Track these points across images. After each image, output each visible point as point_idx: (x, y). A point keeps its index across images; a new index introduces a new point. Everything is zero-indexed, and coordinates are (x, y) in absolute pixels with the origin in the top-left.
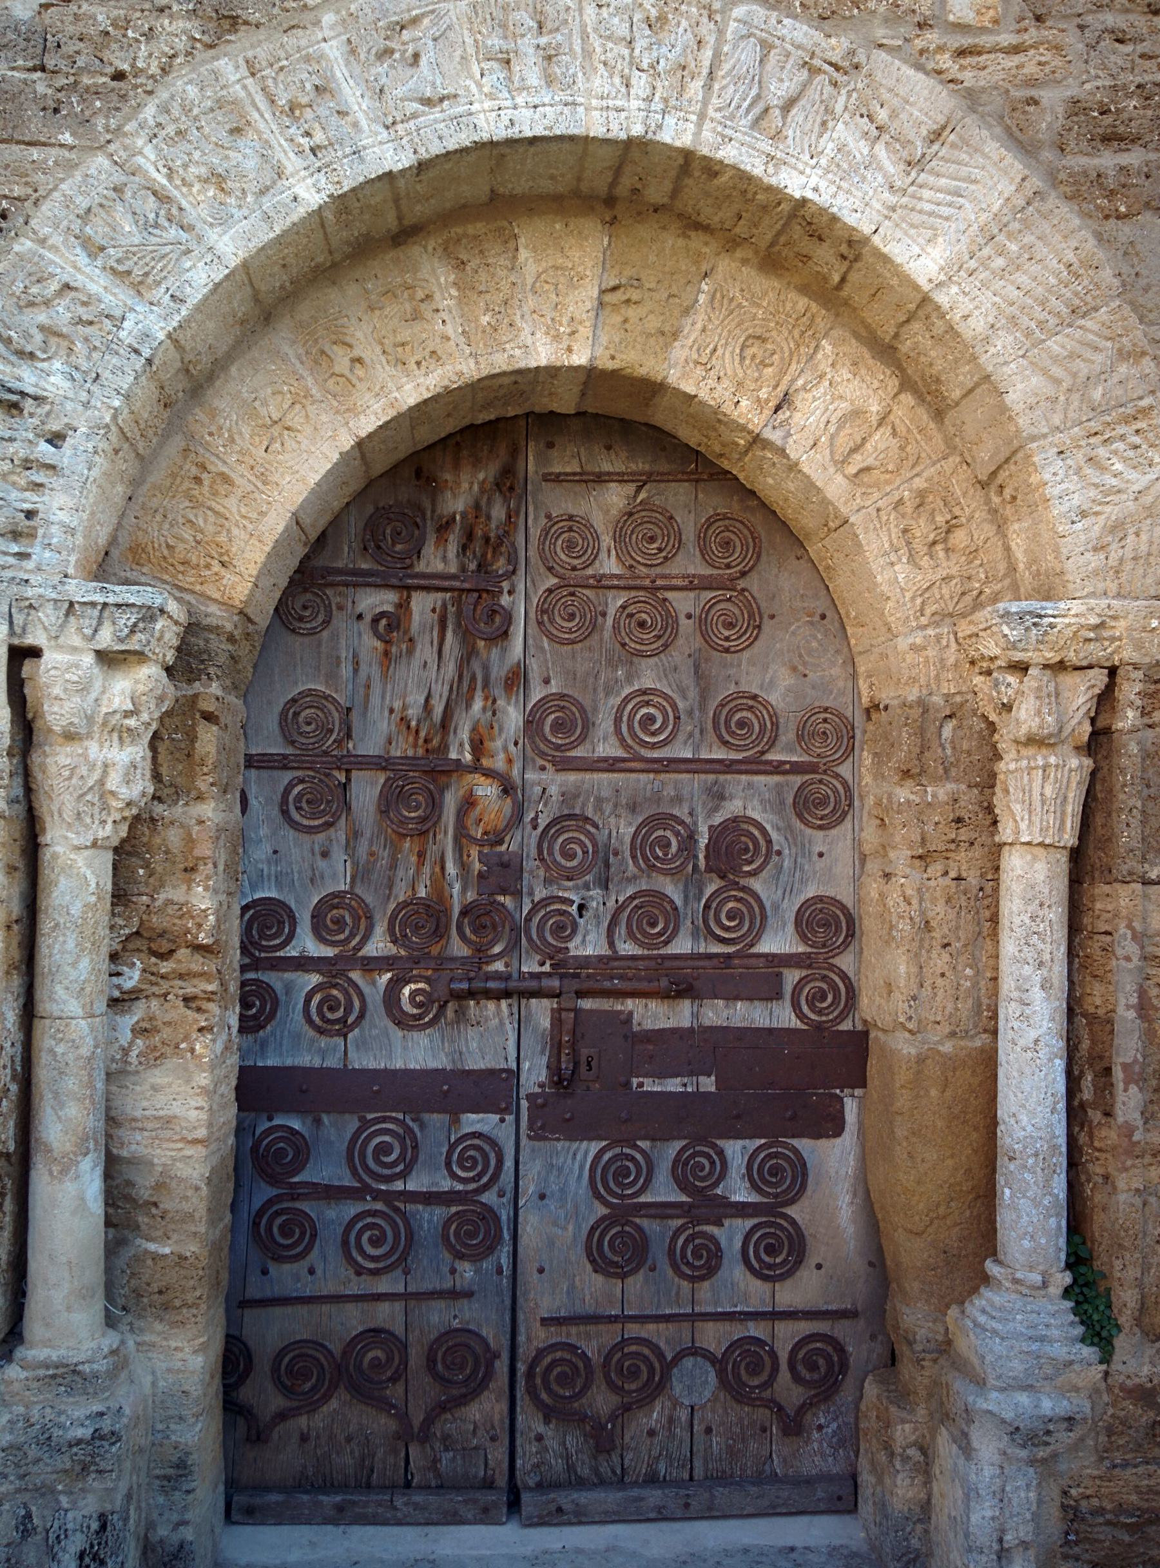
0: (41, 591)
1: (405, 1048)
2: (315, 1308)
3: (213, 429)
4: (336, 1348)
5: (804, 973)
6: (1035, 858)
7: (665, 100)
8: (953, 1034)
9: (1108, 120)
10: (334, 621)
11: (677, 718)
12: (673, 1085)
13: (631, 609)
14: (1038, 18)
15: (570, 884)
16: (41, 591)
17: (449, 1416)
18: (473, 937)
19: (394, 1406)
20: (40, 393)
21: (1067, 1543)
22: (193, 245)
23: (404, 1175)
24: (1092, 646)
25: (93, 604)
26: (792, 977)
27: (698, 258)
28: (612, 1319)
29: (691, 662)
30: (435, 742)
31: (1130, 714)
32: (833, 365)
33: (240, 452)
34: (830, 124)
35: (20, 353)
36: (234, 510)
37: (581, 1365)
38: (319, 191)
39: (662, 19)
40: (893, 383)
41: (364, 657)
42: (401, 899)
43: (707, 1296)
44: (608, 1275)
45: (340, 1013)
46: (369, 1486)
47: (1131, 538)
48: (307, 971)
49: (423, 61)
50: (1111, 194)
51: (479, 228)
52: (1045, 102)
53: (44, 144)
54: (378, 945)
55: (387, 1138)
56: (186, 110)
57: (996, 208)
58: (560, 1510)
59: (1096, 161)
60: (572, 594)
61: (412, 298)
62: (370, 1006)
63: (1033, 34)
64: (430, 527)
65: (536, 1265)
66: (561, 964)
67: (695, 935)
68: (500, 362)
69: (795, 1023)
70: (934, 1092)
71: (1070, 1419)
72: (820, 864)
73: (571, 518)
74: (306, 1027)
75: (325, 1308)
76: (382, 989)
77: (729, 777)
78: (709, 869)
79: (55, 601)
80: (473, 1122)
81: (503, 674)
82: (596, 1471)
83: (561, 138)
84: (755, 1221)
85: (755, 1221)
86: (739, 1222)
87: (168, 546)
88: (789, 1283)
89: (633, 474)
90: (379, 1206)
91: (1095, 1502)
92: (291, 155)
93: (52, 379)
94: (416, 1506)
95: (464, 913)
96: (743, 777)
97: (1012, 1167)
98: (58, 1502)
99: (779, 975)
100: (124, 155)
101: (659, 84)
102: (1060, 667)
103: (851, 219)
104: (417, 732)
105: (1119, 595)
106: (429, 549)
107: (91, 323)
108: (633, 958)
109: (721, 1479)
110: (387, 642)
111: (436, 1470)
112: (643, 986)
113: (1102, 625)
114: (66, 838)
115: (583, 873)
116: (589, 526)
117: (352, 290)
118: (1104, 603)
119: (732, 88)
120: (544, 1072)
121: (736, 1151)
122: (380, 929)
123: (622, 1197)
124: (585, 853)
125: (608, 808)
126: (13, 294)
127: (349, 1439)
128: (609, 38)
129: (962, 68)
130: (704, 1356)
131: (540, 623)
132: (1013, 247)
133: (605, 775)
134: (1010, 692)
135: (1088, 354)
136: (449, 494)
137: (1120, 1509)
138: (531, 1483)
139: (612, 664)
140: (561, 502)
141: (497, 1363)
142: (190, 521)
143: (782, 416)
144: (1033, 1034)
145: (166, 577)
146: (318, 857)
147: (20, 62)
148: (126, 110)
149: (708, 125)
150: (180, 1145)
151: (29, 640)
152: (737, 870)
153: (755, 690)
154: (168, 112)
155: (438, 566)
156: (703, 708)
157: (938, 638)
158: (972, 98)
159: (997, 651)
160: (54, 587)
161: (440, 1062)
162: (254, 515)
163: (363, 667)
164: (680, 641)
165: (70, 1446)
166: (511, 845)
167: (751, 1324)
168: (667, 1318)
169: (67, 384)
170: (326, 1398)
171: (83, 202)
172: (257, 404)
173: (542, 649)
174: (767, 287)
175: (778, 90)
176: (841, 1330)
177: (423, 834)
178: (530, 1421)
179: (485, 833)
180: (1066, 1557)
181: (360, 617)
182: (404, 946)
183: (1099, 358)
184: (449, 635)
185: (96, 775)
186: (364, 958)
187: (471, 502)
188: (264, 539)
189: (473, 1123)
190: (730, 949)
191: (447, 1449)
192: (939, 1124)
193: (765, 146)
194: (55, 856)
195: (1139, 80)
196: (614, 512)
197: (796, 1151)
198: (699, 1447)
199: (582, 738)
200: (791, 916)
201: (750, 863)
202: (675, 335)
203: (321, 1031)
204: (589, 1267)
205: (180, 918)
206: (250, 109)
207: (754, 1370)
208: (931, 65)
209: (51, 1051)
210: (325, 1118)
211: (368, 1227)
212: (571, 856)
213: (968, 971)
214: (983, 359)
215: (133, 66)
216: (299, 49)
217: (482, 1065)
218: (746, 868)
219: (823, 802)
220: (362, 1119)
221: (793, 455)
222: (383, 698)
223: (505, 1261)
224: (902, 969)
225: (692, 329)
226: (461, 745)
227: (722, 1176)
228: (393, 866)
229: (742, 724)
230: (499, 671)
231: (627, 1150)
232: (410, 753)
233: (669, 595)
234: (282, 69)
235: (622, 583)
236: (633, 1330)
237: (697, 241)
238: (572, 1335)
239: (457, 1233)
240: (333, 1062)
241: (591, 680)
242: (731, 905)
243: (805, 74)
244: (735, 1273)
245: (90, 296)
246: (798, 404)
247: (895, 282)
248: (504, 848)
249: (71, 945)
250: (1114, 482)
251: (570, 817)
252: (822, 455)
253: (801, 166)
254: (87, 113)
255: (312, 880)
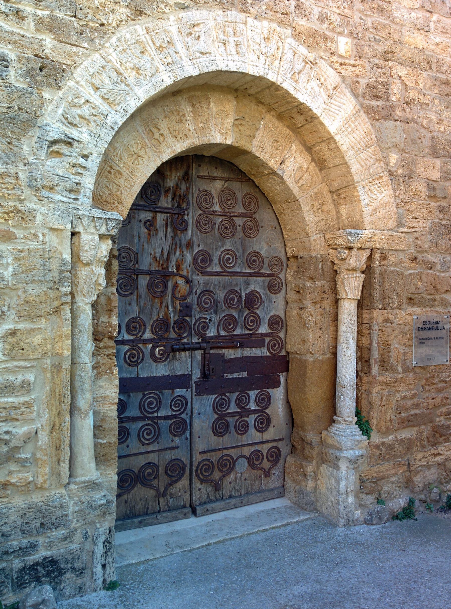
0: (83, 212)
1: (157, 369)
2: (129, 458)
3: (115, 154)
4: (136, 471)
5: (270, 338)
6: (351, 303)
7: (269, 65)
8: (323, 354)
9: (375, 91)
10: (132, 222)
11: (236, 259)
12: (236, 375)
13: (223, 223)
14: (359, 57)
15: (207, 313)
16: (83, 212)
17: (172, 487)
18: (177, 331)
19: (155, 487)
20: (80, 140)
21: (361, 489)
22: (130, 92)
23: (157, 411)
24: (369, 243)
25: (101, 218)
26: (267, 340)
27: (261, 113)
28: (219, 450)
29: (240, 240)
30: (165, 265)
31: (377, 262)
32: (295, 152)
33: (124, 163)
34: (310, 80)
35: (71, 124)
36: (123, 184)
37: (211, 465)
38: (170, 79)
39: (268, 39)
40: (310, 159)
41: (142, 236)
42: (155, 319)
43: (246, 439)
44: (218, 436)
45: (135, 359)
46: (147, 514)
47: (378, 213)
48: (124, 345)
49: (201, 39)
50: (375, 113)
51: (198, 93)
52: (361, 83)
53: (77, 46)
54: (148, 335)
55: (152, 399)
56: (126, 42)
57: (349, 113)
58: (207, 510)
59: (372, 103)
60: (206, 217)
61: (178, 115)
62: (145, 356)
63: (358, 62)
64: (162, 191)
65: (198, 436)
66: (204, 339)
67: (241, 328)
68: (205, 140)
69: (268, 354)
70: (317, 371)
71: (362, 456)
72: (274, 305)
73: (206, 191)
74: (125, 364)
75: (132, 458)
76: (149, 350)
77: (250, 278)
78: (246, 307)
79: (88, 216)
80: (179, 392)
81: (185, 243)
82: (216, 497)
83: (240, 72)
84: (258, 415)
85: (258, 415)
86: (253, 415)
87: (100, 195)
88: (266, 432)
89: (223, 178)
90: (149, 422)
91: (367, 477)
92: (161, 65)
93: (83, 135)
94: (165, 517)
95: (175, 323)
96: (254, 278)
97: (344, 390)
98: (96, 526)
99: (264, 339)
100: (105, 55)
101: (267, 60)
102: (361, 249)
103: (315, 111)
104: (159, 262)
105: (376, 229)
106: (162, 198)
107: (96, 116)
108: (225, 336)
109: (248, 493)
110: (149, 230)
111: (168, 505)
112: (229, 345)
113: (372, 237)
114: (83, 300)
115: (210, 309)
116: (211, 195)
117: (160, 109)
118: (372, 231)
119: (286, 65)
120: (199, 374)
121: (252, 394)
122: (148, 329)
123: (222, 411)
124: (211, 302)
125: (217, 287)
126: (68, 101)
127: (141, 500)
128: (254, 42)
129: (342, 69)
130: (244, 457)
131: (197, 226)
132: (353, 125)
133: (216, 277)
134: (345, 255)
135: (369, 159)
136: (168, 180)
137: (373, 478)
138: (198, 504)
139: (218, 241)
140: (203, 185)
141: (186, 468)
142: (107, 187)
143: (283, 166)
144: (350, 352)
145: (100, 206)
146: (127, 305)
147: (68, 13)
148: (106, 38)
149: (280, 75)
150: (109, 405)
151: (77, 230)
152: (253, 307)
153: (258, 251)
154: (120, 41)
155: (165, 205)
156: (243, 256)
157: (320, 237)
158: (343, 77)
159: (343, 243)
160: (88, 211)
161: (166, 373)
162: (129, 186)
163: (142, 239)
164: (237, 234)
165: (99, 507)
166: (189, 300)
167: (256, 446)
168: (234, 447)
169: (89, 137)
170: (133, 487)
171: (92, 70)
172: (129, 146)
173: (197, 234)
174: (278, 124)
175: (298, 68)
176: (279, 444)
177: (162, 297)
178: (197, 484)
179: (181, 296)
180: (361, 493)
181: (140, 221)
182: (156, 335)
183: (372, 160)
184: (169, 229)
185: (95, 279)
186: (144, 340)
187: (175, 183)
188: (133, 195)
189: (179, 392)
190: (251, 332)
191: (171, 498)
192: (318, 380)
193: (294, 84)
194: (79, 307)
195: (382, 80)
196: (218, 190)
197: (268, 393)
198: (243, 485)
199: (209, 265)
200: (267, 321)
201: (256, 305)
202: (254, 137)
203: (130, 365)
204: (213, 434)
205: (106, 327)
206: (147, 45)
207: (257, 460)
208: (334, 67)
209: (80, 375)
210: (131, 394)
211: (146, 429)
212: (206, 303)
213: (327, 336)
214: (346, 158)
215: (108, 22)
216: (163, 27)
217: (180, 373)
218: (255, 307)
219: (275, 286)
220: (143, 394)
221: (285, 179)
222: (148, 249)
223: (188, 436)
224: (311, 336)
225: (259, 135)
226: (173, 266)
227: (249, 403)
228: (152, 308)
229: (254, 261)
230: (184, 242)
231: (223, 397)
232: (157, 269)
233: (234, 218)
234: (157, 33)
235: (221, 214)
236: (225, 452)
237: (261, 106)
238: (208, 456)
239: (174, 428)
240: (134, 375)
241: (212, 246)
242: (251, 318)
243: (303, 64)
244: (252, 431)
245: (96, 106)
246: (286, 163)
247: (322, 131)
248: (186, 301)
249: (85, 338)
250: (375, 196)
251: (207, 291)
252: (292, 180)
253: (303, 92)
254: (93, 37)
255: (126, 313)
